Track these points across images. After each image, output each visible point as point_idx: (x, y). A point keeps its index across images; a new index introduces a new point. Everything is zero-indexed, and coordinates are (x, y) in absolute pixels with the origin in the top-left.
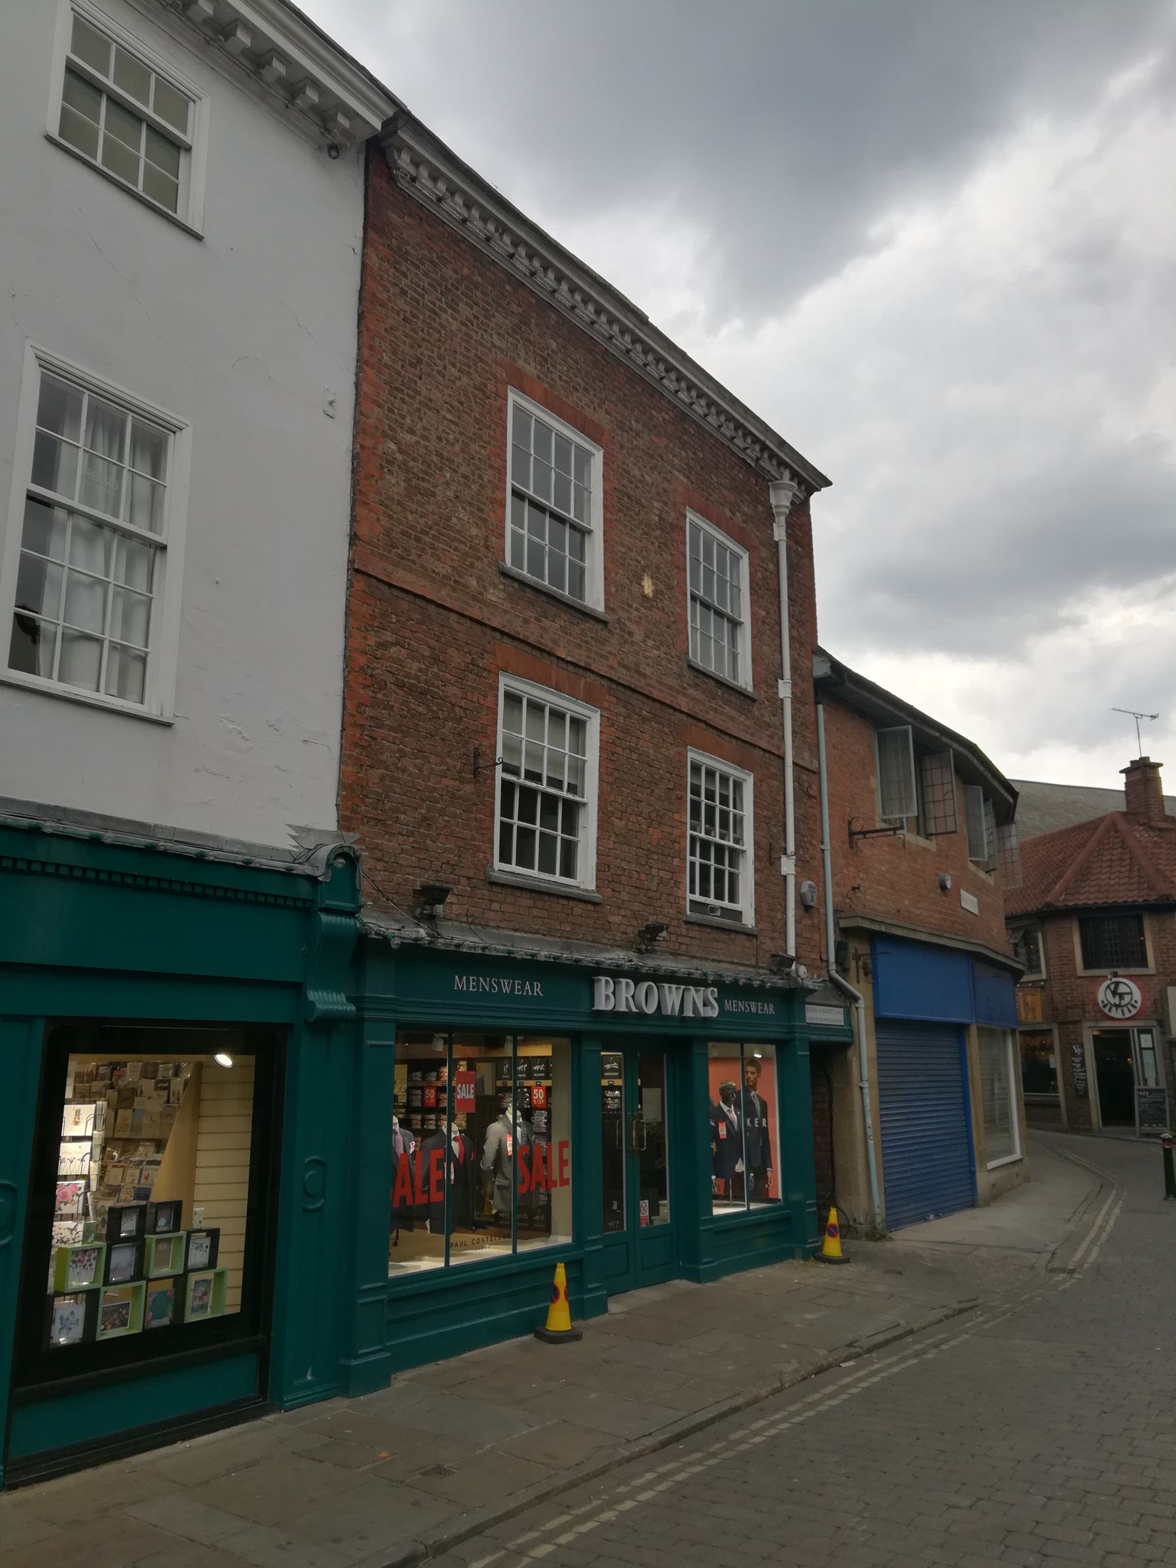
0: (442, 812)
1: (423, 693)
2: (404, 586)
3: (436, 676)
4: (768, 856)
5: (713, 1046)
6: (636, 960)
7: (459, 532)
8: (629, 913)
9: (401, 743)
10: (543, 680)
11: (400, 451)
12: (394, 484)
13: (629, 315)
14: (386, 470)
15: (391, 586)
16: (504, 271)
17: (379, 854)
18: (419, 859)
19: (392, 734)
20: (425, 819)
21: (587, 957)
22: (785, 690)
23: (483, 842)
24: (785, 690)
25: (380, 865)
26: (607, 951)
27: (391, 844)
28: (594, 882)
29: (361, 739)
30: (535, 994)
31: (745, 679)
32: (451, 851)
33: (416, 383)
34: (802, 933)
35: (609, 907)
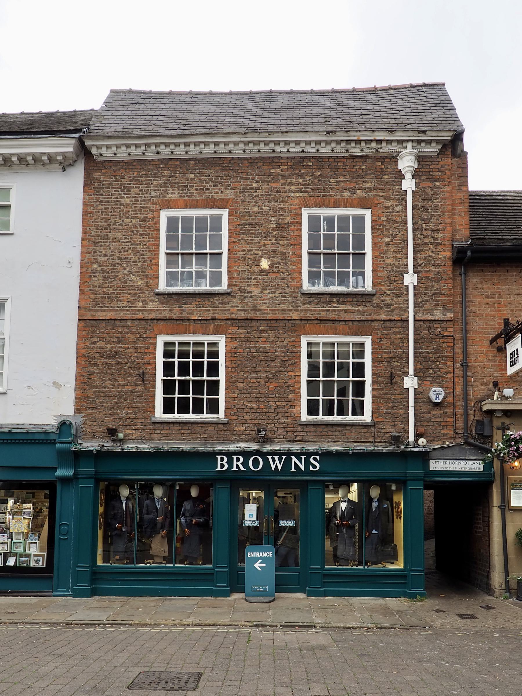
0: (126, 399)
1: (114, 356)
2: (101, 318)
3: (121, 347)
5: (480, 468)
7: (132, 286)
8: (251, 425)
9: (103, 377)
10: (187, 332)
12: (98, 280)
13: (233, 136)
14: (93, 277)
16: (159, 160)
17: (94, 420)
18: (114, 419)
19: (98, 375)
20: (116, 403)
21: (211, 448)
23: (149, 407)
25: (95, 424)
26: (234, 443)
27: (100, 415)
32: (131, 413)
35: (235, 424)
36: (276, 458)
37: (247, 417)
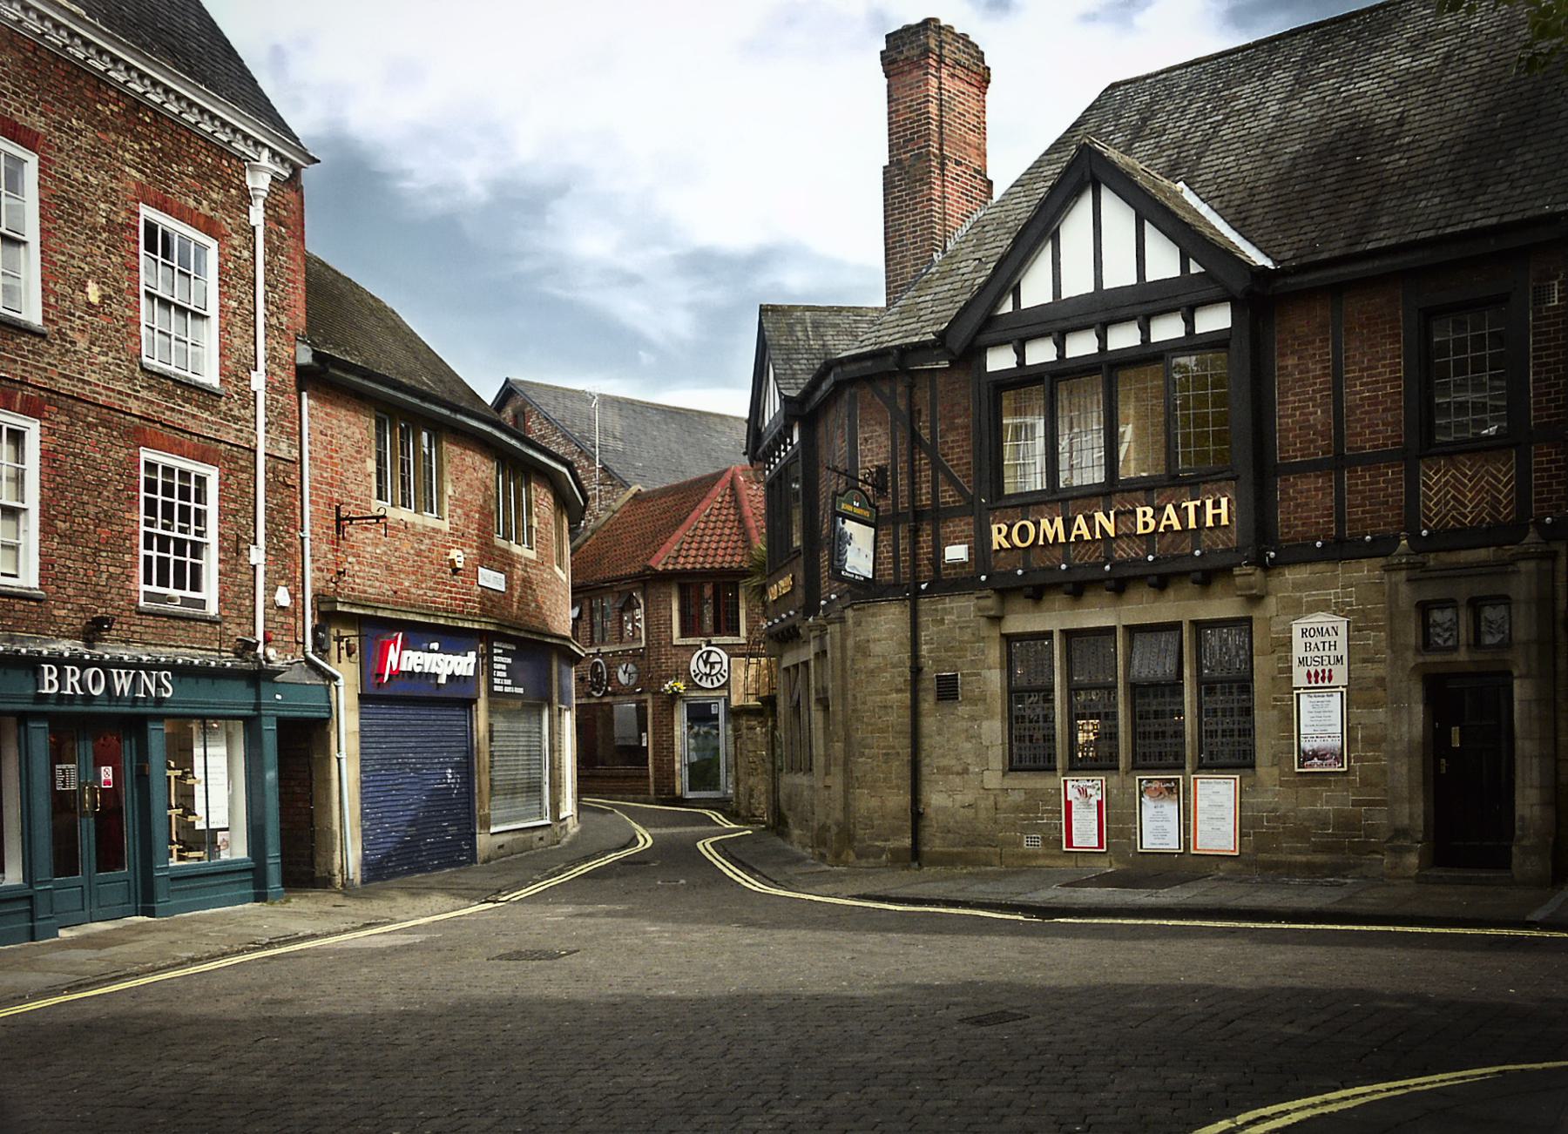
4: (234, 548)
22: (258, 381)
24: (258, 381)
31: (210, 376)
36: (123, 672)
37: (70, 591)
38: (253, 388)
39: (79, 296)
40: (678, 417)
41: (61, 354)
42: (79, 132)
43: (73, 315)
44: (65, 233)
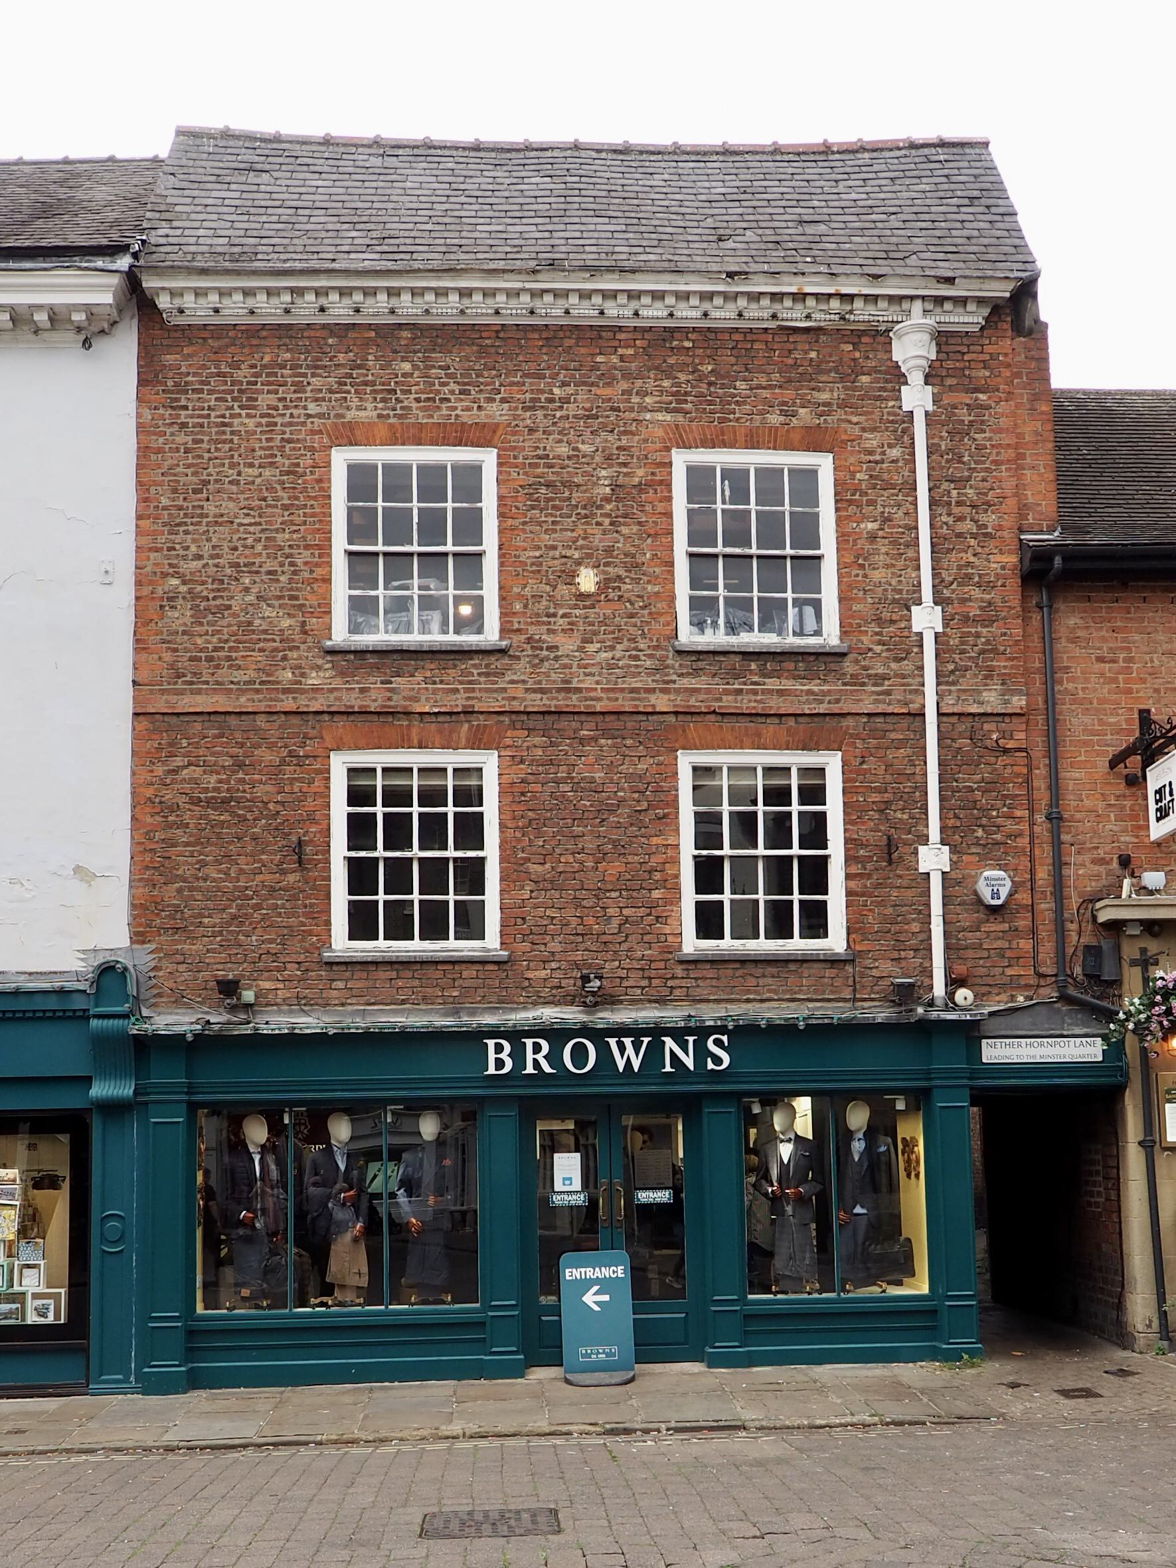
0: (257, 907)
1: (225, 801)
6: (583, 1018)
7: (265, 632)
8: (564, 965)
11: (184, 583)
13: (506, 276)
15: (178, 714)
16: (324, 326)
17: (180, 958)
25: (182, 968)
26: (525, 1009)
27: (194, 947)
28: (499, 940)
29: (151, 862)
30: (530, 1069)
32: (271, 941)
33: (202, 507)
34: (981, 944)
36: (628, 1041)
37: (555, 946)
38: (915, 629)
39: (563, 590)
40: (590, 259)
41: (534, 666)
42: (566, 400)
43: (554, 615)
44: (540, 524)
